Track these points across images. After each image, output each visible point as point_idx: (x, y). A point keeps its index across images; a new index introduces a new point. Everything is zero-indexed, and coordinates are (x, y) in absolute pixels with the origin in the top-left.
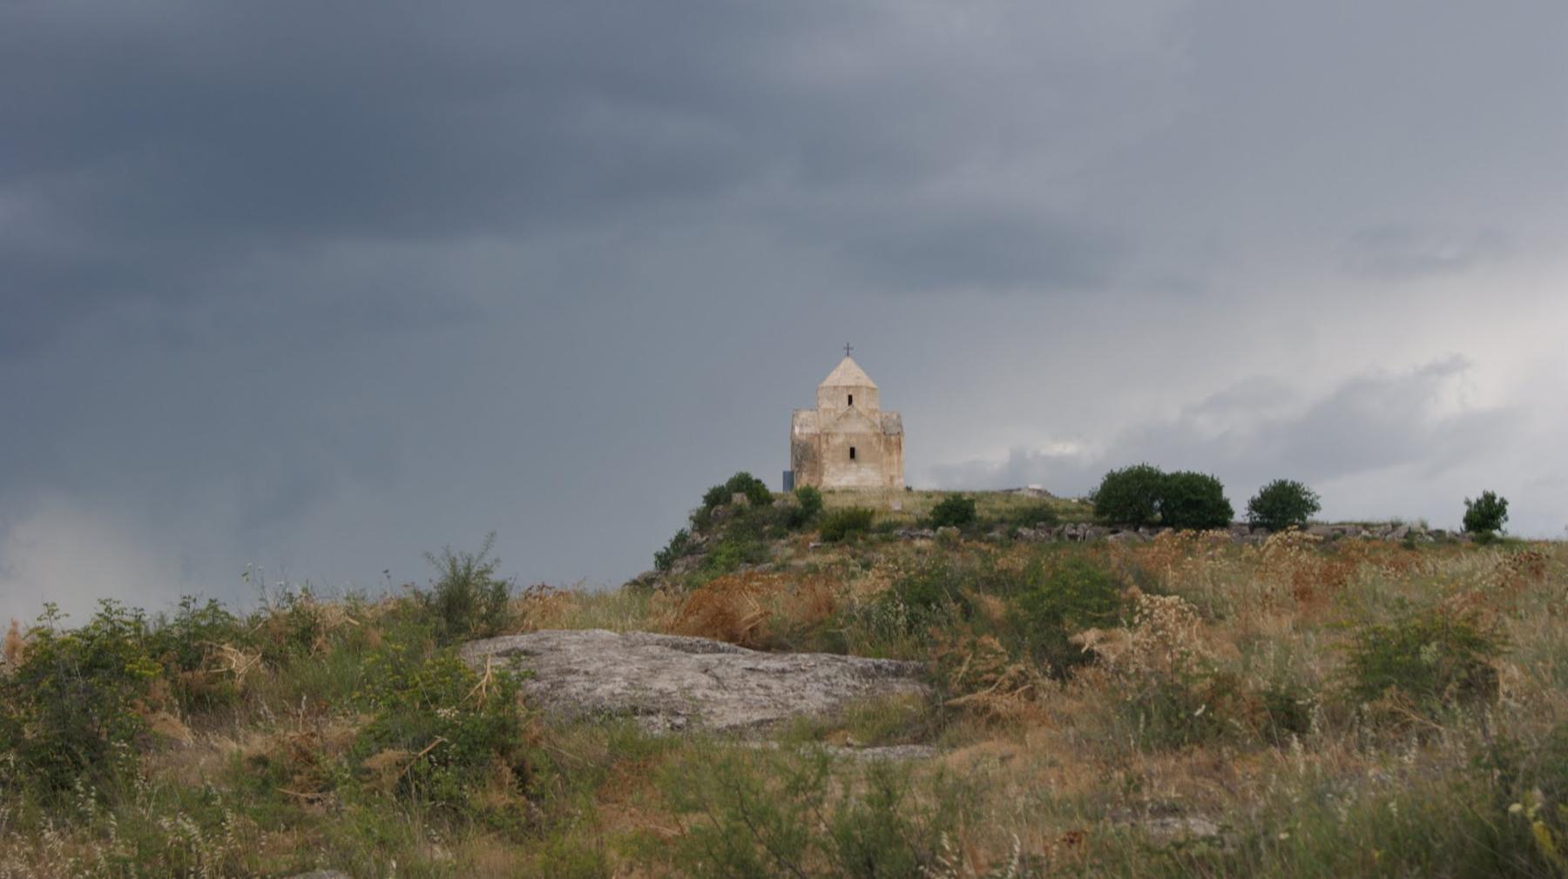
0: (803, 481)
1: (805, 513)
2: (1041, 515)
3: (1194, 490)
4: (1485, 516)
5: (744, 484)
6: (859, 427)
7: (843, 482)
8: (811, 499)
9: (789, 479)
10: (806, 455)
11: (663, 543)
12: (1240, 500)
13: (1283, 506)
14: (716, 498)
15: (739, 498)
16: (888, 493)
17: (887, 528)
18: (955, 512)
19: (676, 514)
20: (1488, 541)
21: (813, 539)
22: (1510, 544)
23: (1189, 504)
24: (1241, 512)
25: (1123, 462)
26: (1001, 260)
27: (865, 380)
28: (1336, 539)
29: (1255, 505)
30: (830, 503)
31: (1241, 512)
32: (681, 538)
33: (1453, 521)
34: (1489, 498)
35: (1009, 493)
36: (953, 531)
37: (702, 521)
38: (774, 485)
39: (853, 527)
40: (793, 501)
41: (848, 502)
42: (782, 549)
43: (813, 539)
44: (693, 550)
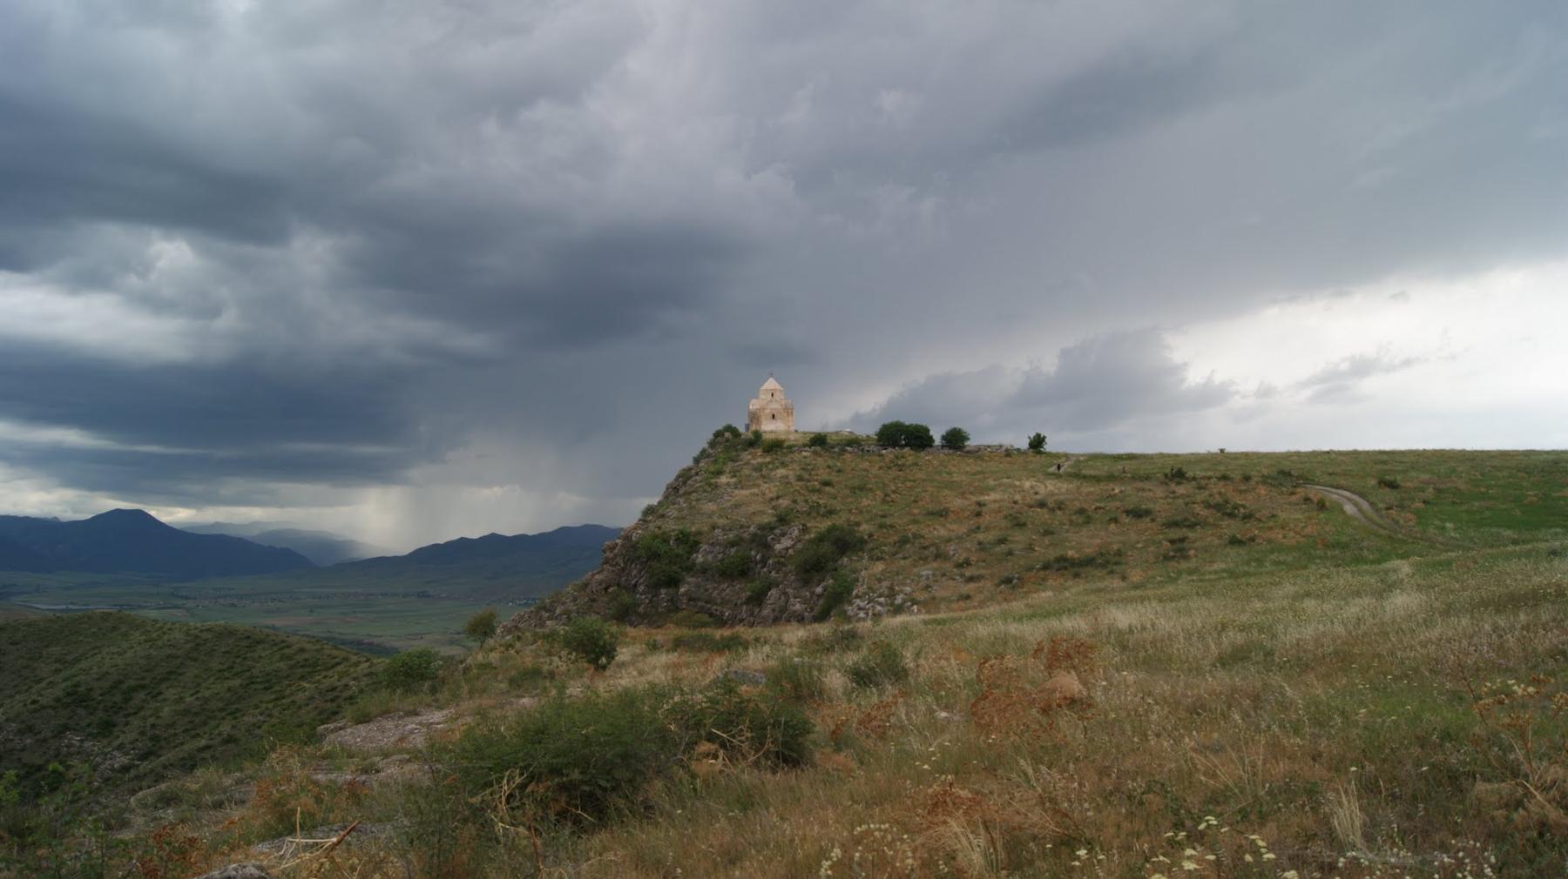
0: (753, 428)
1: (755, 441)
2: (854, 442)
3: (1286, 465)
4: (1037, 443)
5: (729, 429)
6: (775, 406)
7: (769, 428)
8: (758, 435)
9: (747, 427)
10: (754, 417)
11: (696, 453)
12: (937, 435)
13: (955, 440)
14: (718, 434)
15: (727, 435)
16: (788, 432)
17: (790, 447)
18: (819, 441)
19: (701, 441)
20: (1040, 453)
21: (759, 452)
22: (1049, 455)
23: (917, 438)
24: (938, 441)
25: (888, 421)
26: (773, 357)
27: (778, 387)
28: (977, 453)
29: (944, 438)
30: (766, 437)
31: (938, 441)
32: (704, 451)
33: (1023, 444)
34: (1038, 435)
35: (837, 433)
36: (818, 448)
37: (712, 444)
38: (742, 430)
39: (775, 447)
40: (750, 435)
41: (773, 436)
42: (746, 456)
43: (759, 452)
44: (709, 456)
